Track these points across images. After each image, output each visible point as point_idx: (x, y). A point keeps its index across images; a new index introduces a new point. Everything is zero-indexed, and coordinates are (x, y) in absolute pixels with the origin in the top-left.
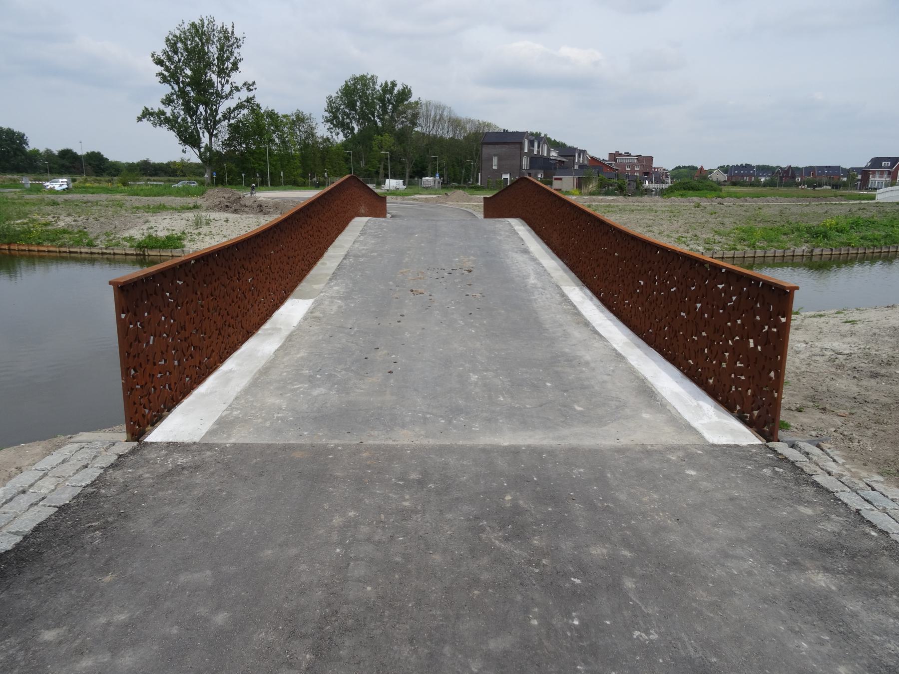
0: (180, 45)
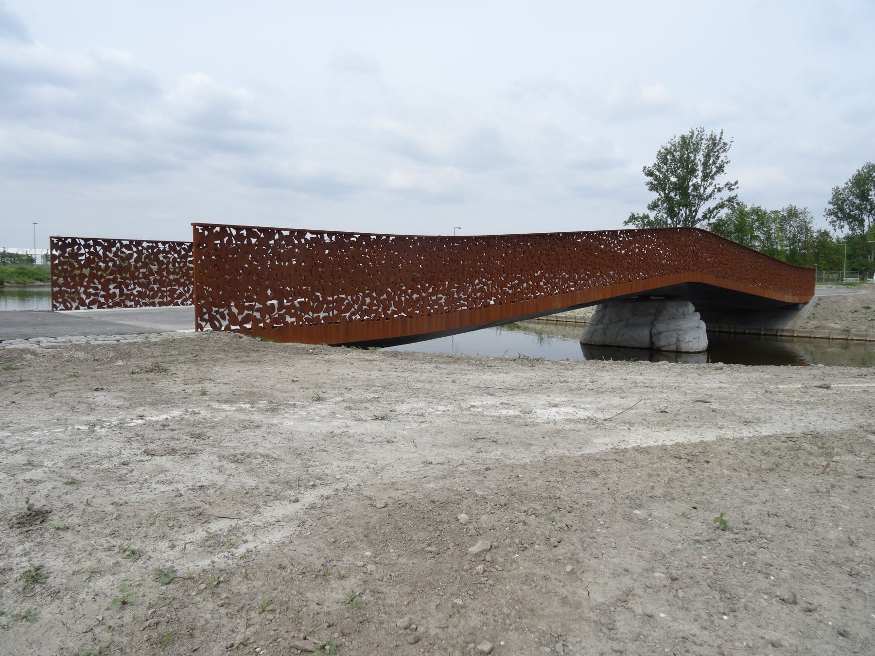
0: (669, 157)
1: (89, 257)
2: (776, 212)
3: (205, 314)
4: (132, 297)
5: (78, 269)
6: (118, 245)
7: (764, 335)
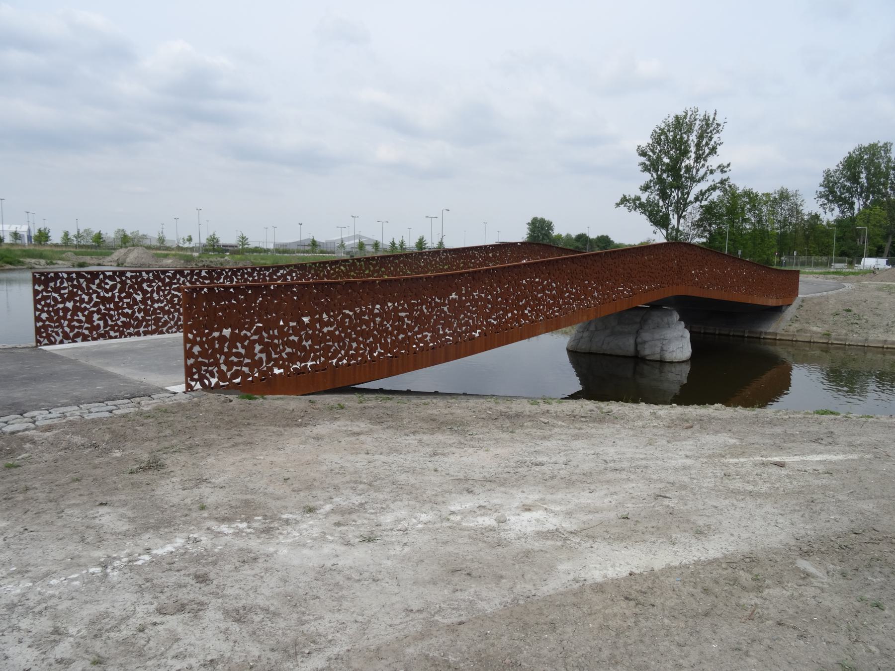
0: (662, 137)
1: (72, 290)
2: (768, 195)
3: (195, 374)
4: (116, 328)
5: (61, 303)
6: (101, 276)
7: (748, 337)
